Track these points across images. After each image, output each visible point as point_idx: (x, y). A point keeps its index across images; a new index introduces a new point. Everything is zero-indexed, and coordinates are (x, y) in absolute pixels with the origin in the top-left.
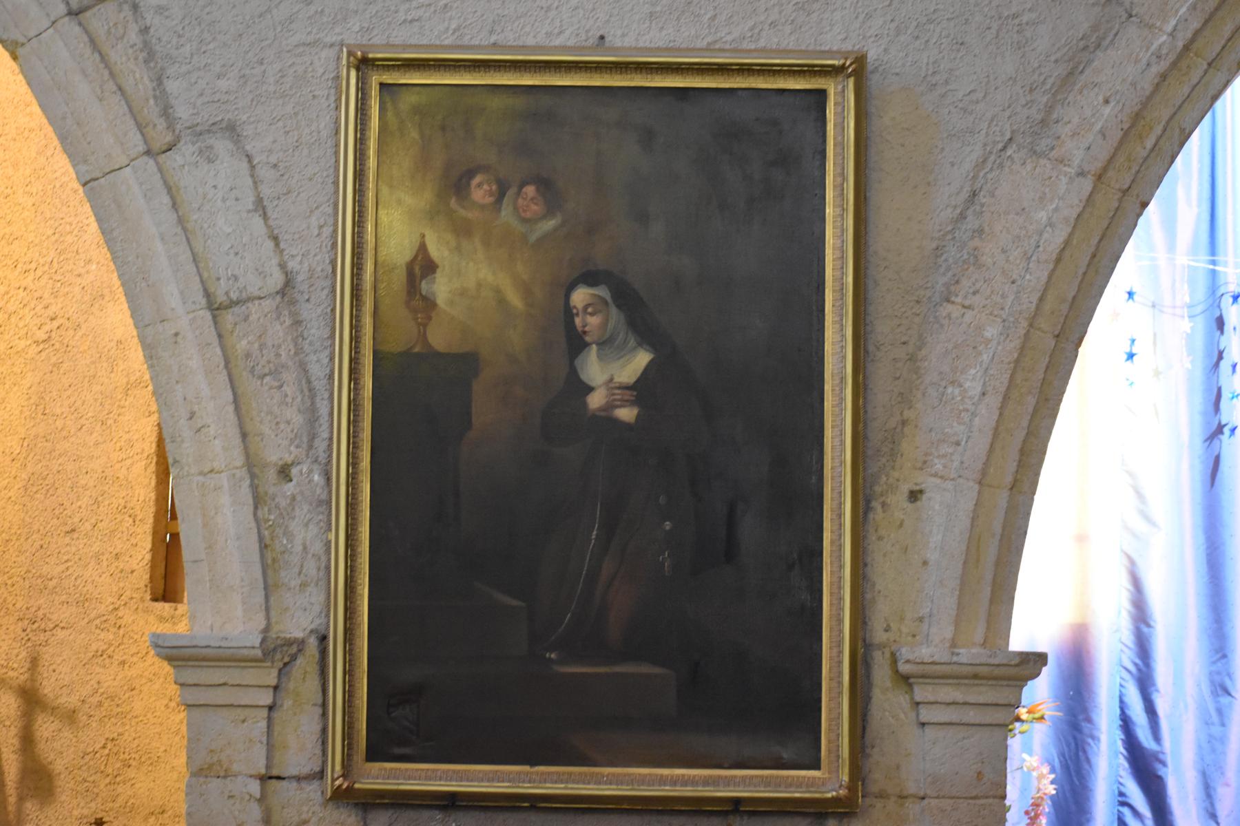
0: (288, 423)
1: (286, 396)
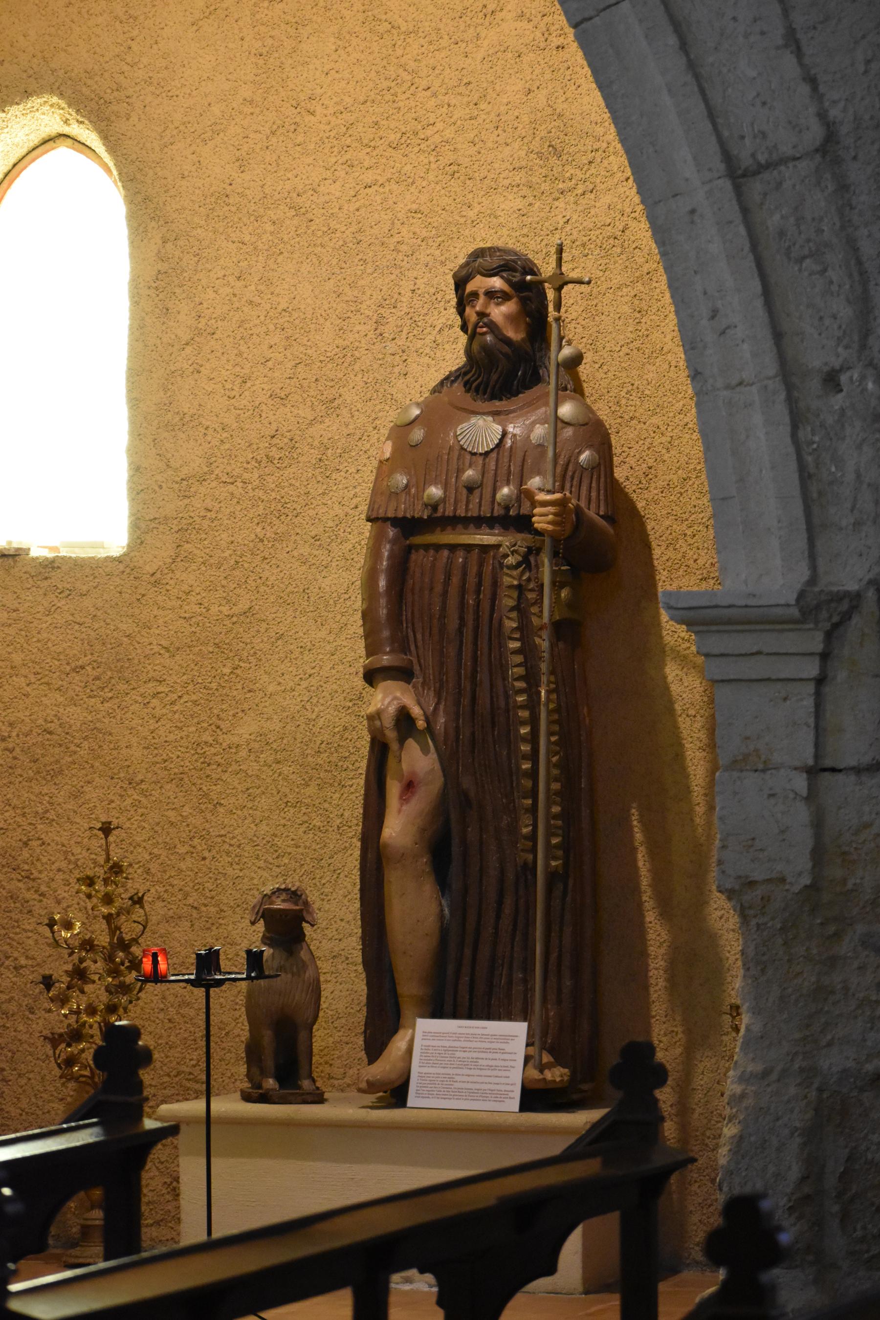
0: (835, 317)
1: (831, 282)
